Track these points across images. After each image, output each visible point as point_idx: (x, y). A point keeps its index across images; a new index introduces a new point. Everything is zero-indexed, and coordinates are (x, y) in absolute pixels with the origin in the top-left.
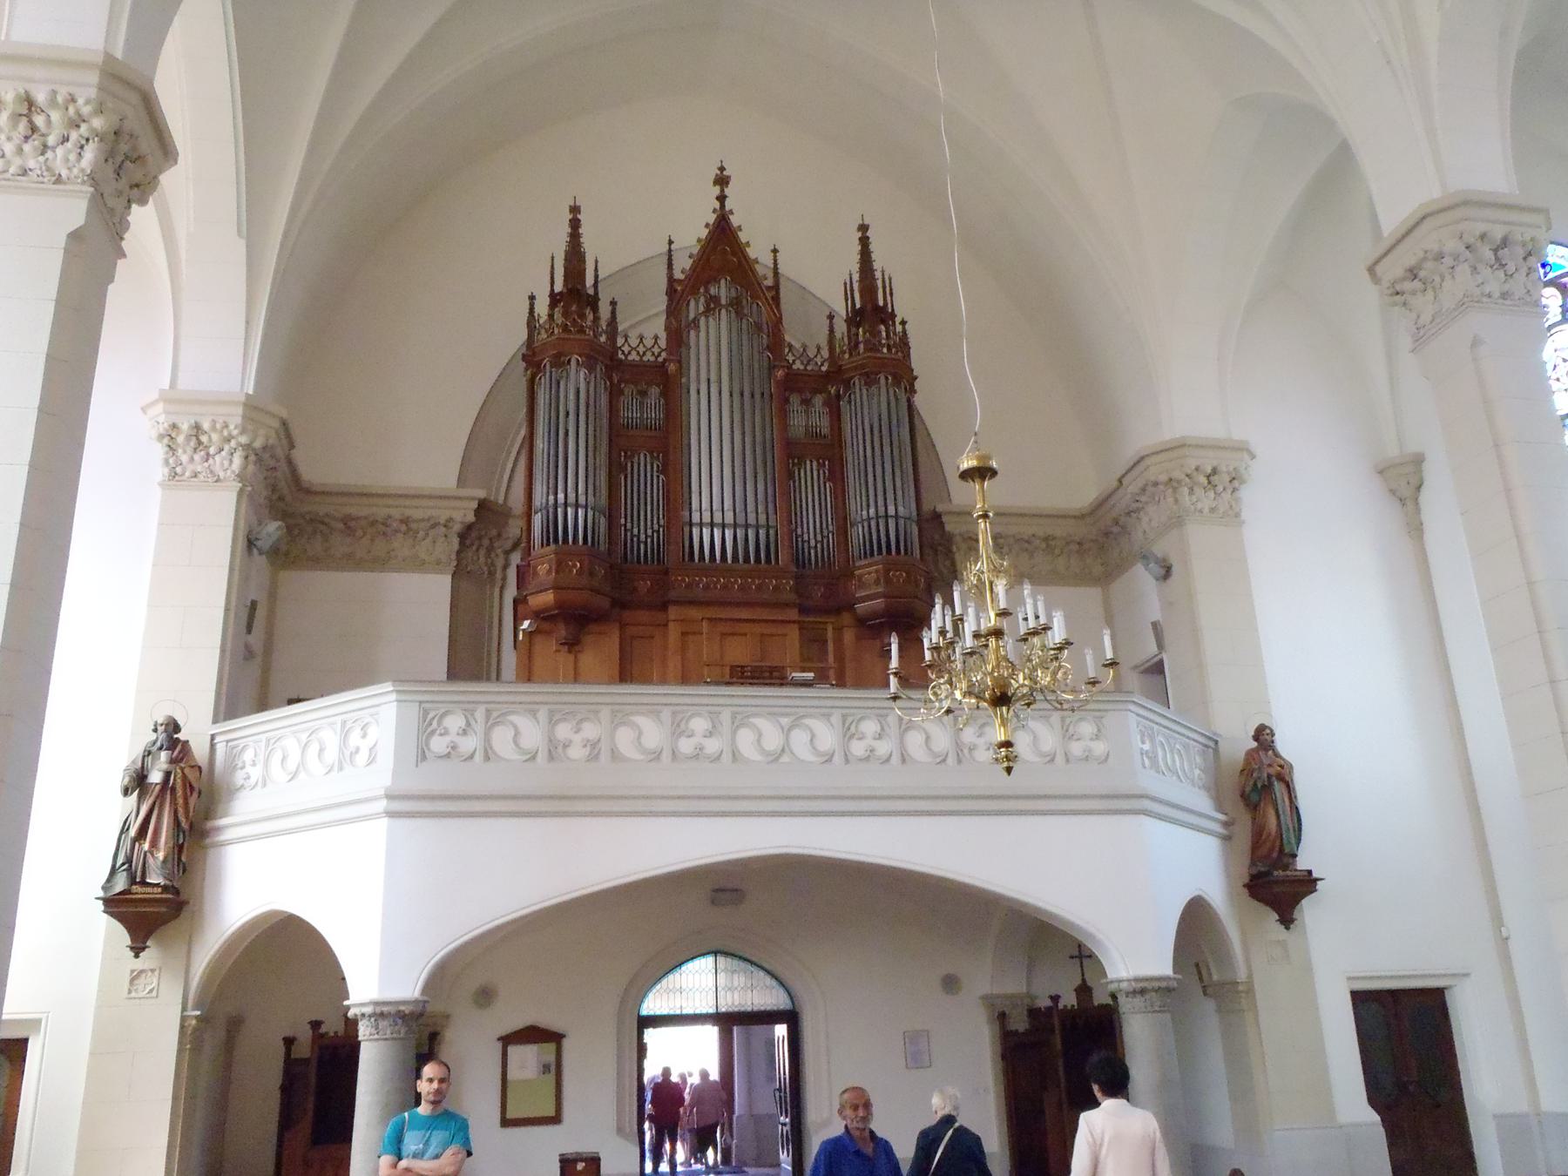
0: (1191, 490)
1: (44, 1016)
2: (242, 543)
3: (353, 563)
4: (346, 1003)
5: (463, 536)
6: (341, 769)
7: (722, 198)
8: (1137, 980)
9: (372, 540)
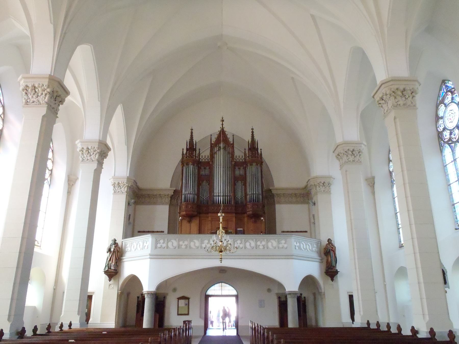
0: (319, 187)
1: (95, 291)
2: (127, 204)
3: (149, 203)
4: (143, 291)
5: (171, 197)
6: (143, 249)
7: (223, 125)
8: (290, 292)
9: (154, 198)
